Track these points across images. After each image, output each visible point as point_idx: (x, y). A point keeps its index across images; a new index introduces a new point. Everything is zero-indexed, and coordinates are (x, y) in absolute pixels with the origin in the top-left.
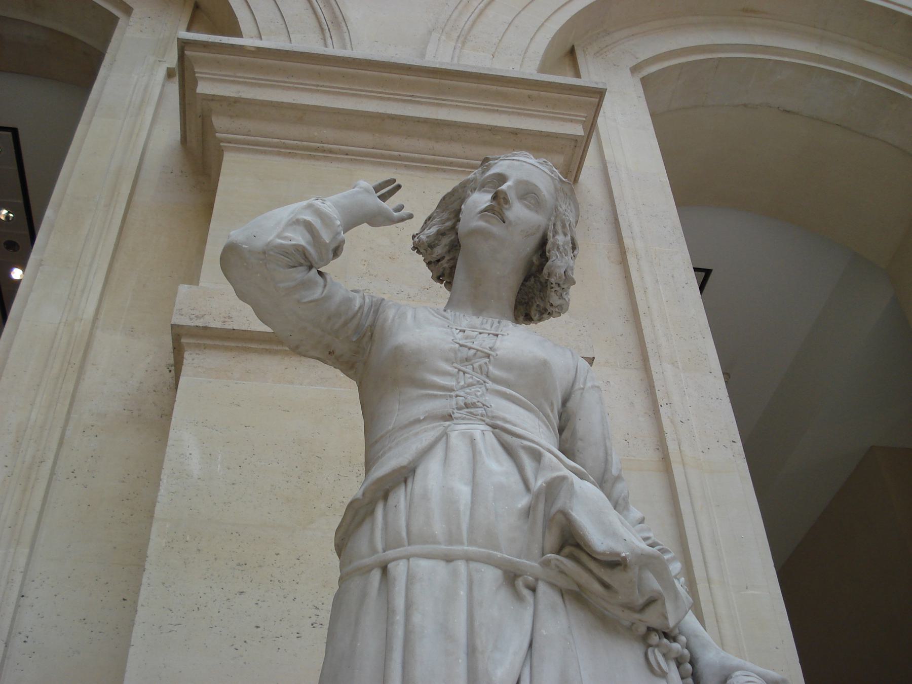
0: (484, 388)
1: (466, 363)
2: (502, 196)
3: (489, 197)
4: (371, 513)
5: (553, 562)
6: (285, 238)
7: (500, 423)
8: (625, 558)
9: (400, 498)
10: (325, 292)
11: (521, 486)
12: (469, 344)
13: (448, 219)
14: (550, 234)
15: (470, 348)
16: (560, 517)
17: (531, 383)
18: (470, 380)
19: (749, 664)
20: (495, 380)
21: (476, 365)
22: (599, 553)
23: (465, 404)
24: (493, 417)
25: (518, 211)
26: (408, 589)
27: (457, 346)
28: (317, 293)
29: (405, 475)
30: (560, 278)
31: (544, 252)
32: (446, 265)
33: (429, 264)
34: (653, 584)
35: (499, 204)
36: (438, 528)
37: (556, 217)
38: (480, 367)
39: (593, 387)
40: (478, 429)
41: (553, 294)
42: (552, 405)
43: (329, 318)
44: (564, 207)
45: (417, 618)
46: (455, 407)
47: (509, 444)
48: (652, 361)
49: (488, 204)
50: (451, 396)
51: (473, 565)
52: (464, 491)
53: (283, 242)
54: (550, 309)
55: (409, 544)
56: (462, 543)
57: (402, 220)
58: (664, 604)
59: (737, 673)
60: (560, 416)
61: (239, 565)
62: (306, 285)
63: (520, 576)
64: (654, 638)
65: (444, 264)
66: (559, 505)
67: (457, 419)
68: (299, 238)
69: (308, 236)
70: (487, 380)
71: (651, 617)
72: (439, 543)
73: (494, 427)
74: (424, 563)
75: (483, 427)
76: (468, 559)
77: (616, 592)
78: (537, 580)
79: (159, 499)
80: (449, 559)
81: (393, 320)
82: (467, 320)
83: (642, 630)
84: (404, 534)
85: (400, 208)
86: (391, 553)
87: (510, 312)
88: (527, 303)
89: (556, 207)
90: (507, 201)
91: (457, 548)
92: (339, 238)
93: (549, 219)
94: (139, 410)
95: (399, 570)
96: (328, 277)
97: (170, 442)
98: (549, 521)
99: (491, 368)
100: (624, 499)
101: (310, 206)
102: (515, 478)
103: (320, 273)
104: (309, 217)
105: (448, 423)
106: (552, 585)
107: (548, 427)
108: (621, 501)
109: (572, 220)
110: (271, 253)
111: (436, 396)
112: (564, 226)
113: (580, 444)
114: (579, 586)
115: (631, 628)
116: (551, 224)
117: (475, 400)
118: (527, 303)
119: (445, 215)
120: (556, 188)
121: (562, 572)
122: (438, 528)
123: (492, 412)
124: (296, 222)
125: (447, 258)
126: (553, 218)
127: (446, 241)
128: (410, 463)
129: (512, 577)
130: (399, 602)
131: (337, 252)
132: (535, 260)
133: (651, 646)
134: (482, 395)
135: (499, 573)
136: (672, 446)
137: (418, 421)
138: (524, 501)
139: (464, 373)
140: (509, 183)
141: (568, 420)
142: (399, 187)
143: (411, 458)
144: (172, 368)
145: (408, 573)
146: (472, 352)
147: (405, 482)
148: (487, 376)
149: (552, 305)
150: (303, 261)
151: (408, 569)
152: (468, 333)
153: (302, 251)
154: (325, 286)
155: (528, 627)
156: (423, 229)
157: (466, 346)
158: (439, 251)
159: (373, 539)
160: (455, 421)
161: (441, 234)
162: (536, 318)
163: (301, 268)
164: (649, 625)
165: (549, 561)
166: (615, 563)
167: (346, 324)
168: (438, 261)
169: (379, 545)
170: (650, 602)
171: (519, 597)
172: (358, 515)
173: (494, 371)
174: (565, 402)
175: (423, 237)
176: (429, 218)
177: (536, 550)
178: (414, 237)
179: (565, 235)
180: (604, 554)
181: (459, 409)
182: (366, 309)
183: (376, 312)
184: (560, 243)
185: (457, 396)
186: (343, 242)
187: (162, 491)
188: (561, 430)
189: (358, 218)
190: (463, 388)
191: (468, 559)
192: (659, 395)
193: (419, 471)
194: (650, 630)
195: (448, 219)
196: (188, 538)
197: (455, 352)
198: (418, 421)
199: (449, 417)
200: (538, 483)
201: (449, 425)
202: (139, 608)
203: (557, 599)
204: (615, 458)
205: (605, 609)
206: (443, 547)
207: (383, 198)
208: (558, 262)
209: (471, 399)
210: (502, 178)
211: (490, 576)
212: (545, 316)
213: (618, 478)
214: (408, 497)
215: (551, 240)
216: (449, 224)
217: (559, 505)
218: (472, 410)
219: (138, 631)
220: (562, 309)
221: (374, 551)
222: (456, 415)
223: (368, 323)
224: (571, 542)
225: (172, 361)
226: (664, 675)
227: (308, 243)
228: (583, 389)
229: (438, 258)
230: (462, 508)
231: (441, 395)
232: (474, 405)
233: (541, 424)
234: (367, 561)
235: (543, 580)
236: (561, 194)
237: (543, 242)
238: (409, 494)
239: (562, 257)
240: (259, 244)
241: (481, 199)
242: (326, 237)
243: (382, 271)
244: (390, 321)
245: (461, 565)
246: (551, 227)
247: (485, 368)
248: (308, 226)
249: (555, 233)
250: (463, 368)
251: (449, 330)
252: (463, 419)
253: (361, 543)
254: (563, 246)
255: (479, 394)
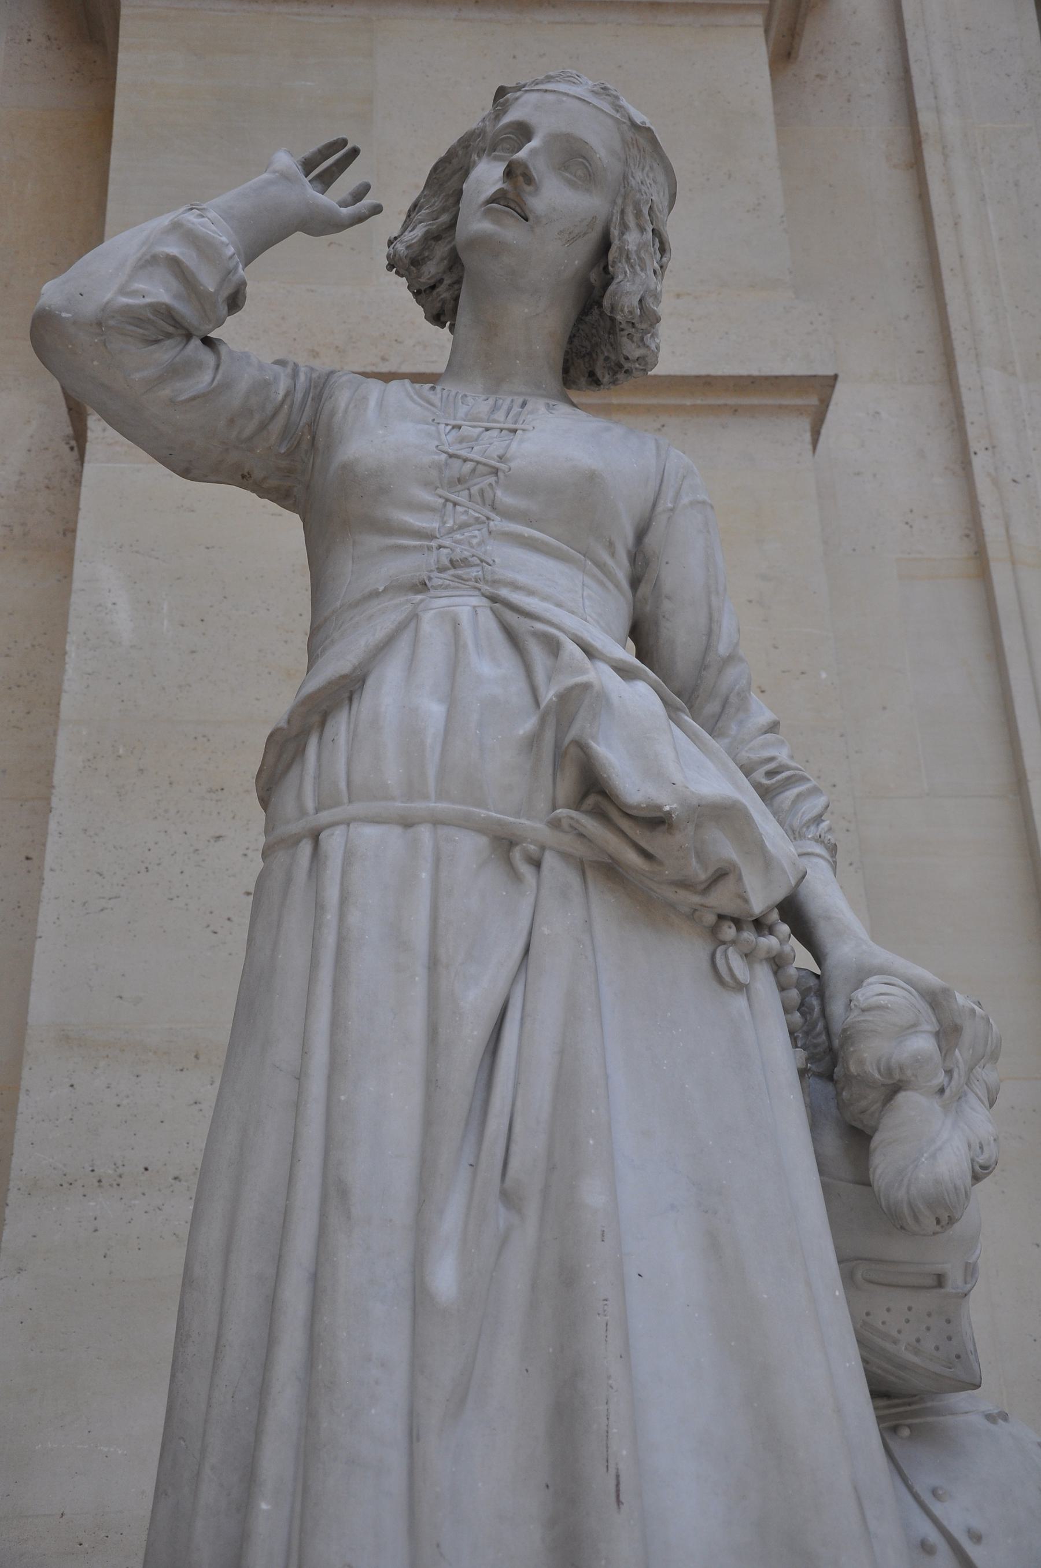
0: (485, 530)
1: (459, 487)
2: (519, 172)
3: (499, 169)
4: (301, 751)
5: (565, 823)
6: (134, 293)
7: (504, 592)
8: (669, 814)
9: (340, 726)
10: (218, 377)
11: (527, 699)
12: (464, 453)
13: (444, 210)
14: (615, 232)
15: (465, 460)
16: (573, 750)
17: (570, 512)
18: (464, 518)
19: (900, 963)
20: (508, 515)
21: (475, 490)
22: (631, 807)
23: (451, 561)
24: (495, 582)
25: (555, 196)
26: (344, 873)
27: (444, 456)
28: (203, 380)
29: (349, 689)
30: (631, 313)
31: (606, 269)
32: (446, 295)
33: (417, 294)
34: (725, 848)
35: (516, 187)
36: (393, 774)
37: (625, 197)
38: (482, 492)
39: (693, 504)
40: (467, 606)
41: (625, 340)
42: (611, 546)
43: (232, 421)
44: (639, 175)
45: (354, 918)
46: (434, 567)
47: (518, 631)
48: (961, 368)
49: (499, 185)
50: (430, 548)
51: (443, 831)
52: (434, 710)
53: (130, 301)
54: (627, 365)
55: (350, 802)
56: (426, 797)
57: (360, 219)
58: (740, 879)
59: (872, 979)
60: (633, 559)
61: (210, 791)
62: (176, 371)
63: (517, 844)
64: (729, 931)
65: (443, 293)
66: (573, 733)
67: (435, 588)
68: (158, 290)
69: (175, 284)
70: (492, 515)
71: (721, 899)
72: (393, 799)
73: (493, 599)
74: (370, 832)
75: (476, 601)
76: (437, 822)
77: (661, 863)
78: (543, 848)
79: (66, 686)
80: (407, 823)
81: (346, 411)
82: (473, 401)
83: (710, 919)
84: (343, 785)
85: (363, 191)
86: (325, 817)
87: (552, 381)
88: (590, 354)
89: (625, 177)
90: (529, 179)
91: (420, 806)
92: (235, 279)
93: (614, 202)
94: (23, 524)
95: (334, 842)
96: (223, 350)
97: (76, 585)
98: (559, 756)
99: (499, 493)
100: (738, 694)
101: (176, 226)
102: (518, 686)
103: (207, 341)
104: (174, 250)
105: (419, 597)
106: (565, 856)
107: (601, 584)
108: (733, 699)
109: (660, 198)
110: (111, 322)
111: (404, 549)
112: (638, 215)
113: (667, 605)
114: (610, 856)
115: (693, 915)
116: (617, 210)
117: (466, 554)
118: (590, 354)
119: (438, 203)
120: (624, 141)
121: (581, 835)
122: (393, 774)
123: (493, 572)
124: (151, 261)
125: (447, 281)
126: (619, 201)
127: (441, 250)
128: (355, 669)
129: (504, 844)
130: (332, 894)
131: (235, 302)
132: (594, 277)
133: (724, 943)
134: (479, 544)
135: (483, 841)
136: (992, 529)
137: (375, 594)
138: (528, 725)
139: (455, 504)
140: (534, 143)
141: (647, 564)
142: (355, 152)
143: (356, 662)
144: (73, 443)
145: (346, 845)
146: (469, 466)
147: (350, 699)
148: (493, 508)
149: (627, 359)
150: (171, 329)
151: (347, 842)
152: (466, 430)
153: (166, 313)
154: (217, 367)
155: (524, 924)
156: (405, 228)
157: (457, 457)
158: (431, 270)
159: (680, 632)
160: (433, 593)
161: (432, 238)
162: (606, 379)
163: (168, 342)
164: (720, 912)
165: (559, 820)
166: (657, 821)
167: (263, 426)
168: (433, 287)
169: (310, 804)
170: (720, 875)
171: (516, 877)
172: (285, 751)
173: (505, 498)
174: (641, 534)
175: (400, 247)
176: (415, 207)
177: (542, 804)
178: (390, 243)
179: (642, 230)
180: (638, 807)
181: (441, 570)
182: (299, 396)
183: (319, 398)
184: (632, 247)
185: (440, 547)
186: (243, 284)
187: (70, 672)
188: (635, 583)
189: (263, 237)
190: (451, 531)
191: (437, 822)
192: (972, 432)
193: (370, 682)
194: (721, 917)
195: (444, 210)
196: (121, 752)
197: (440, 468)
198: (375, 594)
199: (423, 587)
200: (549, 695)
201: (422, 601)
202: (47, 874)
203: (573, 879)
204: (727, 626)
205: (651, 889)
206: (398, 804)
207: (326, 180)
208: (627, 289)
209: (461, 552)
210: (523, 132)
211: (469, 848)
212: (621, 376)
213: (730, 659)
214: (352, 726)
215: (616, 244)
216: (445, 218)
217: (573, 733)
218: (459, 572)
219: (47, 913)
220: (646, 364)
221: (303, 812)
222: (436, 582)
223: (304, 420)
224: (593, 789)
225: (69, 430)
226: (741, 987)
227: (177, 297)
228: (672, 510)
229: (432, 282)
230: (429, 741)
231: (415, 547)
232: (465, 563)
233: (588, 581)
234: (295, 828)
235: (552, 849)
236: (634, 151)
237: (605, 245)
238: (353, 719)
239: (635, 273)
240: (90, 308)
241: (487, 176)
242: (209, 281)
243: (331, 314)
244: (340, 414)
245: (425, 832)
246: (616, 219)
247: (489, 494)
248: (175, 264)
249: (624, 228)
250: (452, 497)
251: (433, 428)
252: (447, 587)
253: (286, 801)
254: (638, 252)
255: (475, 541)
